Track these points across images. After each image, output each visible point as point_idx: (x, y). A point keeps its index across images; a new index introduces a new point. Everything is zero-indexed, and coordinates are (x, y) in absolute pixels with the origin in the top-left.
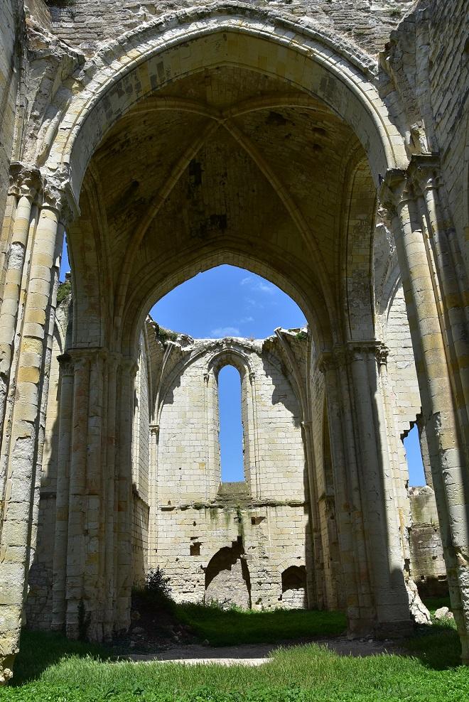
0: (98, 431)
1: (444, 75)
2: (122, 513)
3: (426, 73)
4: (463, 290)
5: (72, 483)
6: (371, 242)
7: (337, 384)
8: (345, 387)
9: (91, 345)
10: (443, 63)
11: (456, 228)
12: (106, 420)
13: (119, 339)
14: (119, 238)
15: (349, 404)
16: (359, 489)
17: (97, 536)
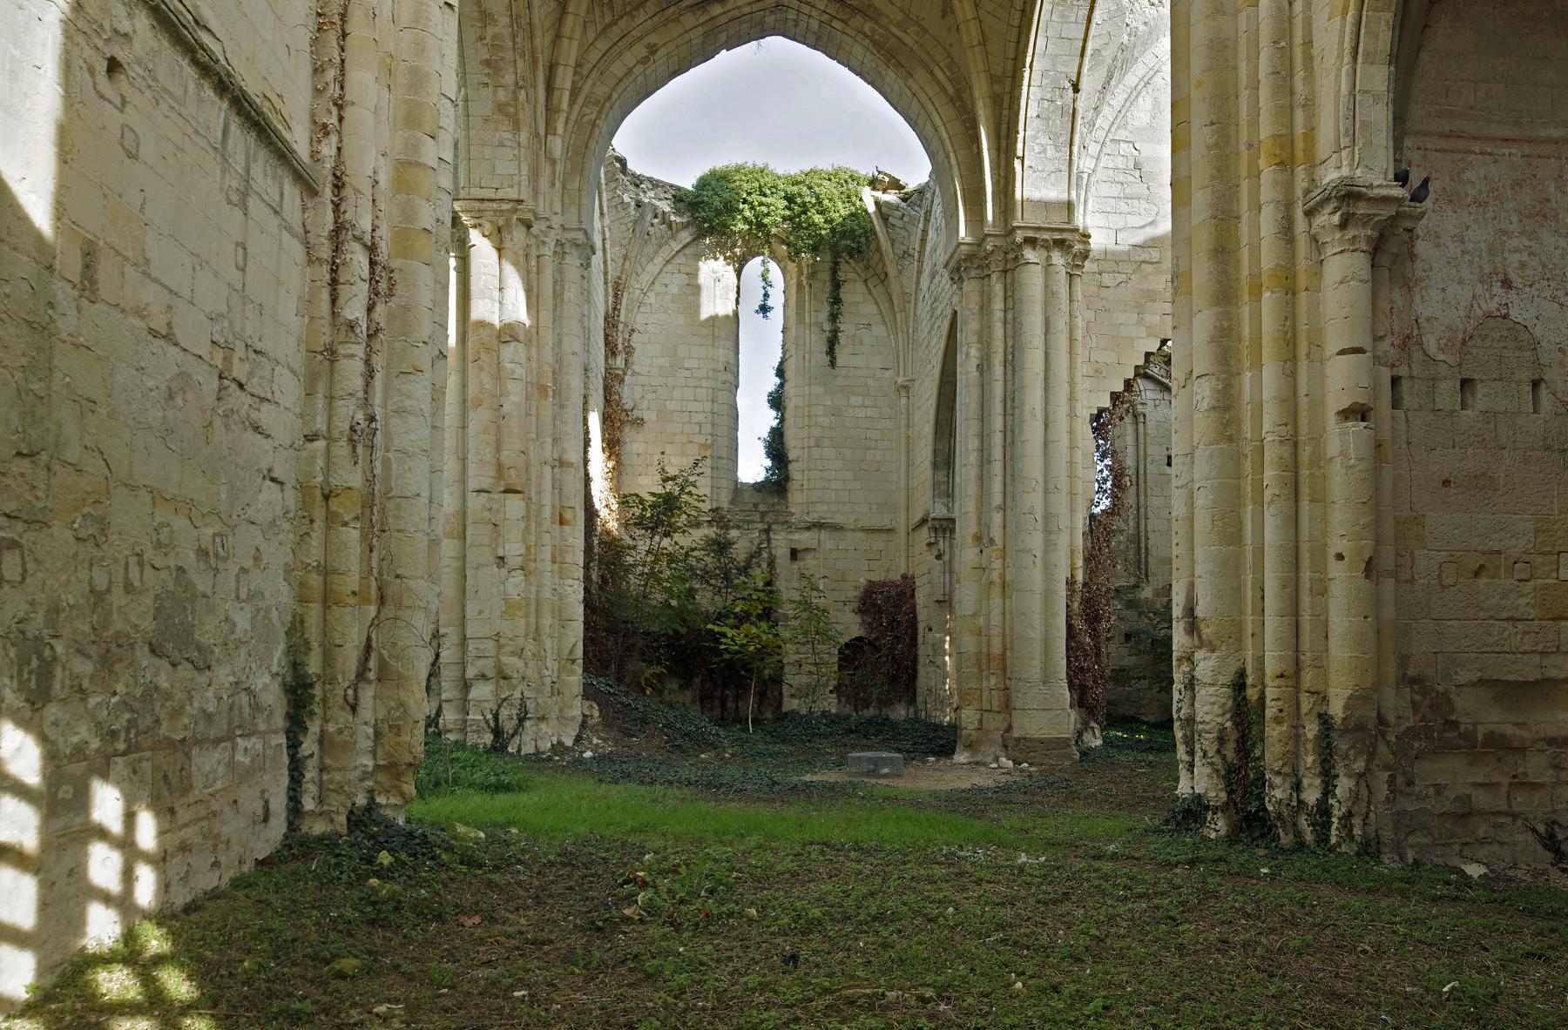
0: (519, 371)
2: (566, 528)
4: (1300, 129)
5: (472, 471)
7: (982, 308)
9: (500, 194)
12: (534, 350)
13: (558, 184)
15: (1001, 350)
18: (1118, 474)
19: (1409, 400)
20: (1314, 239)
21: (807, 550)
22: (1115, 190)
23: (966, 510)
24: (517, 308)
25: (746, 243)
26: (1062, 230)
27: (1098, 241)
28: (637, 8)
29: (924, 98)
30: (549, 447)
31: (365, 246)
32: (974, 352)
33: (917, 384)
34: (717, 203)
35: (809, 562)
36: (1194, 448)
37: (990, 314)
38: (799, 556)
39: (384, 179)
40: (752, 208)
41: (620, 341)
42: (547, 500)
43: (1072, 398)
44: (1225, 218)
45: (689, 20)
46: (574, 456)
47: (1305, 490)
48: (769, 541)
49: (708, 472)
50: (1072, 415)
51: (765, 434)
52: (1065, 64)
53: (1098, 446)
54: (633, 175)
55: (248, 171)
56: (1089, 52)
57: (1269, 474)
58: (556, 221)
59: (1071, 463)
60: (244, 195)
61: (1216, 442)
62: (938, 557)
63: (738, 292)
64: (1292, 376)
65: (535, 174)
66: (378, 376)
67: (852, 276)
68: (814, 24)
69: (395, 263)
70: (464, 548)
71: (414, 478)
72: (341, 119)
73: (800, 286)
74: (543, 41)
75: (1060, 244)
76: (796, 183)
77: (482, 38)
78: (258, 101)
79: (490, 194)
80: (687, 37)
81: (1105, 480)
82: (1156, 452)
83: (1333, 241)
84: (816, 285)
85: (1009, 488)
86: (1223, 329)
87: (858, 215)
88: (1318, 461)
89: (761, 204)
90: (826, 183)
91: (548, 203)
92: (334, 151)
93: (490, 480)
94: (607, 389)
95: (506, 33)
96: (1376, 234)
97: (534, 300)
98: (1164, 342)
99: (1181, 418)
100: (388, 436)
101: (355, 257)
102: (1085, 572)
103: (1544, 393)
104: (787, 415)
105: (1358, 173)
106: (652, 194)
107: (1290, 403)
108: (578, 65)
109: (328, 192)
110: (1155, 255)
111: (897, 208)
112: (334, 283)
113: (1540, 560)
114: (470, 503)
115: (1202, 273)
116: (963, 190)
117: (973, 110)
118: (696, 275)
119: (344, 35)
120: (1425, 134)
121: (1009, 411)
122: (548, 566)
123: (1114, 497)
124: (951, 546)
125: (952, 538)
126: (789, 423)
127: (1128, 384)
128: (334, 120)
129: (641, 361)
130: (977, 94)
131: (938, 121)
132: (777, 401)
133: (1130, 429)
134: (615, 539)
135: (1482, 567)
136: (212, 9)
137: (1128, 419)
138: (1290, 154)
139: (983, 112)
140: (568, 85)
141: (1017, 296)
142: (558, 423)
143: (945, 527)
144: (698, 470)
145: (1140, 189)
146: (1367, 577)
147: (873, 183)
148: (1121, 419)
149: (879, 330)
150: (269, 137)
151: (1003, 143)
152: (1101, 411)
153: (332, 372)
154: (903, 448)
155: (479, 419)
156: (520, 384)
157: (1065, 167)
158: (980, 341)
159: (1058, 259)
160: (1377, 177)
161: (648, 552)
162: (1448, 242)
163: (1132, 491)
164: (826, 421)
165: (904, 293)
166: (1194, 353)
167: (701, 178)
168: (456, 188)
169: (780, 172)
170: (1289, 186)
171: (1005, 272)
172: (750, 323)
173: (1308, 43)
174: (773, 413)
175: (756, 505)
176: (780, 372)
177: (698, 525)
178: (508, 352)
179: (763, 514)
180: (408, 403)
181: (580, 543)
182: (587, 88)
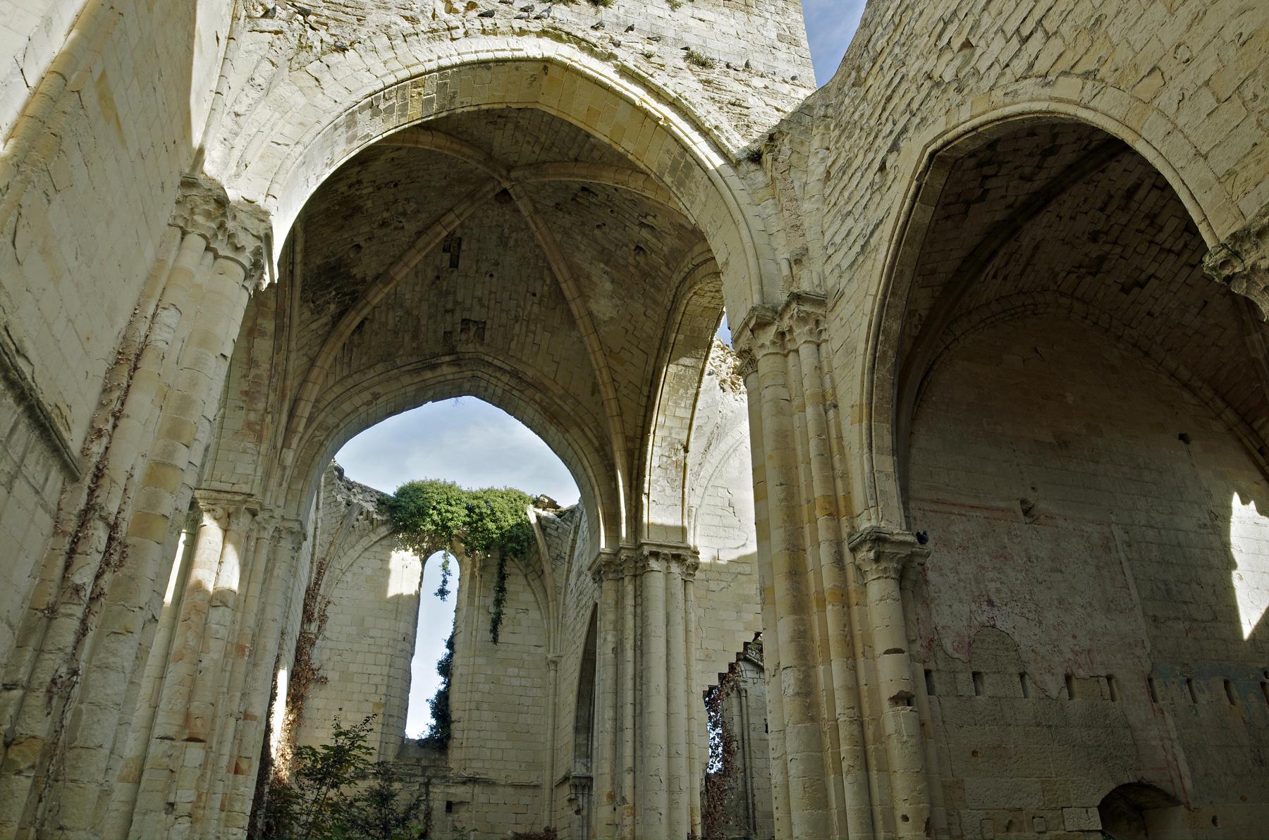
0: (223, 632)
1: (846, 194)
2: (240, 777)
3: (820, 185)
4: (841, 493)
5: (160, 719)
6: (696, 400)
7: (617, 603)
8: (629, 609)
9: (236, 488)
10: (846, 178)
11: (840, 405)
12: (239, 615)
13: (285, 485)
14: (314, 326)
15: (632, 637)
16: (633, 770)
17: (190, 816)
18: (727, 740)
19: (938, 688)
20: (858, 568)
21: (461, 803)
22: (716, 521)
23: (602, 770)
24: (231, 579)
25: (432, 539)
26: (678, 548)
27: (704, 557)
28: (369, 368)
29: (576, 447)
30: (237, 699)
31: (108, 524)
32: (610, 638)
33: (563, 660)
34: (412, 507)
35: (463, 814)
36: (785, 726)
37: (623, 608)
38: (454, 808)
39: (138, 474)
40: (440, 513)
41: (317, 610)
42: (226, 750)
43: (688, 677)
44: (795, 550)
45: (406, 380)
46: (259, 711)
47: (873, 762)
48: (427, 794)
49: (378, 728)
50: (689, 692)
51: (432, 696)
52: (678, 434)
53: (710, 718)
54: (348, 482)
55: (22, 460)
56: (694, 427)
57: (845, 748)
58: (278, 513)
59: (689, 732)
60: (12, 478)
61: (802, 721)
62: (578, 812)
63: (422, 578)
64: (853, 669)
65: (267, 475)
66: (90, 634)
67: (517, 571)
68: (499, 391)
69: (131, 540)
70: (137, 793)
71: (101, 730)
72: (115, 426)
73: (472, 576)
74: (292, 383)
75: (677, 557)
76: (476, 498)
77: (245, 376)
78: (49, 409)
79: (227, 487)
80: (403, 391)
81: (717, 747)
82: (755, 720)
83: (872, 571)
84: (487, 576)
85: (638, 753)
86: (800, 632)
87: (523, 526)
88: (880, 737)
89: (447, 511)
90: (499, 500)
91: (274, 498)
92: (102, 450)
93: (175, 728)
94: (299, 651)
95: (265, 375)
96: (900, 567)
97: (247, 573)
98: (758, 634)
99: (773, 694)
100: (85, 689)
101: (96, 533)
102: (703, 828)
103: (1028, 682)
104: (454, 681)
105: (883, 524)
106: (360, 497)
107: (854, 690)
108: (317, 401)
109: (88, 480)
110: (747, 569)
111: (554, 522)
112: (72, 552)
113: (1050, 815)
114: (152, 750)
115: (781, 588)
116: (604, 514)
117: (613, 458)
118: (388, 562)
119: (135, 368)
120: (922, 500)
121: (638, 687)
122: (216, 814)
123: (725, 761)
124: (589, 802)
125: (590, 795)
126: (454, 688)
127: (732, 667)
128: (109, 427)
129: (331, 628)
130: (615, 448)
131: (587, 464)
132: (445, 668)
133: (735, 701)
134: (285, 787)
135: (1010, 822)
136: (34, 343)
137: (734, 695)
138: (836, 509)
139: (619, 460)
140: (306, 414)
141: (644, 595)
142: (249, 679)
143: (584, 784)
144: (368, 726)
145: (734, 521)
146: (928, 835)
147: (536, 503)
148: (728, 695)
149: (535, 614)
150: (50, 435)
151: (634, 483)
152: (712, 688)
153: (48, 627)
154: (550, 713)
155: (178, 671)
156: (221, 642)
157: (679, 503)
158: (615, 629)
159: (675, 568)
160: (894, 526)
161: (315, 801)
162: (943, 568)
163: (739, 755)
164: (485, 688)
165: (556, 587)
166: (779, 648)
167: (402, 488)
168: (200, 481)
169: (464, 488)
170: (838, 529)
171: (635, 576)
172: (429, 603)
173: (840, 438)
174: (442, 679)
175: (418, 760)
176: (450, 644)
177: (364, 777)
178: (215, 615)
179: (425, 768)
180: (112, 660)
181: (251, 792)
182: (320, 418)
